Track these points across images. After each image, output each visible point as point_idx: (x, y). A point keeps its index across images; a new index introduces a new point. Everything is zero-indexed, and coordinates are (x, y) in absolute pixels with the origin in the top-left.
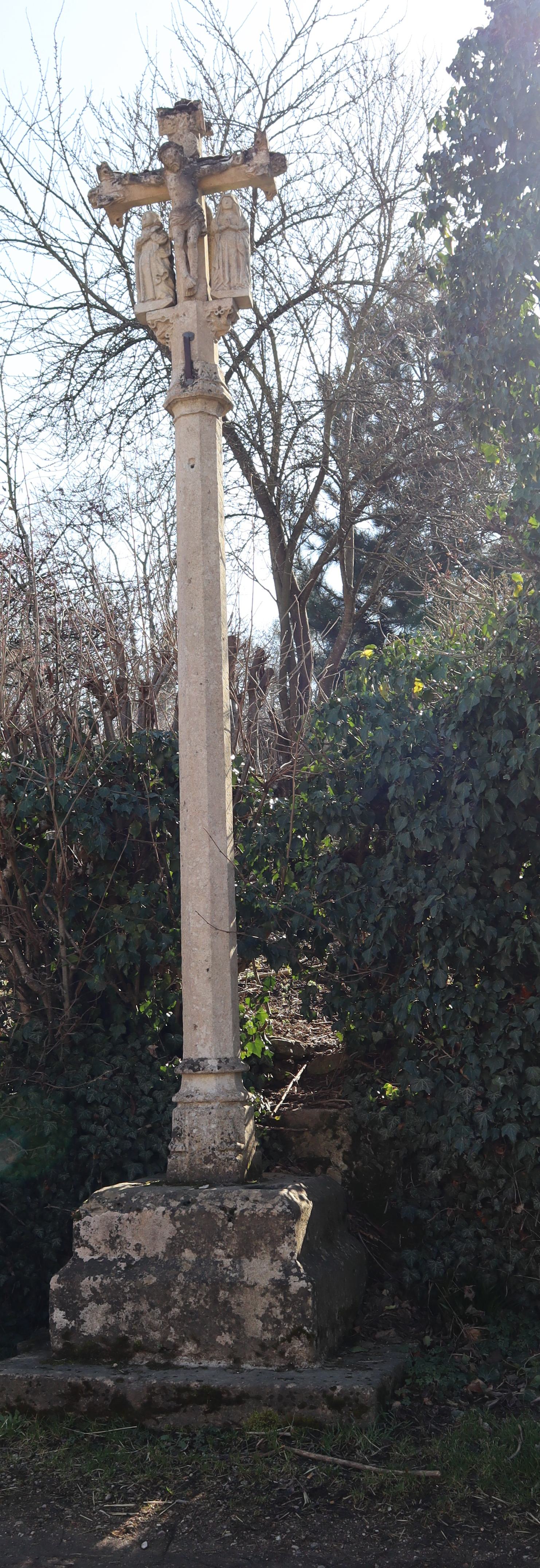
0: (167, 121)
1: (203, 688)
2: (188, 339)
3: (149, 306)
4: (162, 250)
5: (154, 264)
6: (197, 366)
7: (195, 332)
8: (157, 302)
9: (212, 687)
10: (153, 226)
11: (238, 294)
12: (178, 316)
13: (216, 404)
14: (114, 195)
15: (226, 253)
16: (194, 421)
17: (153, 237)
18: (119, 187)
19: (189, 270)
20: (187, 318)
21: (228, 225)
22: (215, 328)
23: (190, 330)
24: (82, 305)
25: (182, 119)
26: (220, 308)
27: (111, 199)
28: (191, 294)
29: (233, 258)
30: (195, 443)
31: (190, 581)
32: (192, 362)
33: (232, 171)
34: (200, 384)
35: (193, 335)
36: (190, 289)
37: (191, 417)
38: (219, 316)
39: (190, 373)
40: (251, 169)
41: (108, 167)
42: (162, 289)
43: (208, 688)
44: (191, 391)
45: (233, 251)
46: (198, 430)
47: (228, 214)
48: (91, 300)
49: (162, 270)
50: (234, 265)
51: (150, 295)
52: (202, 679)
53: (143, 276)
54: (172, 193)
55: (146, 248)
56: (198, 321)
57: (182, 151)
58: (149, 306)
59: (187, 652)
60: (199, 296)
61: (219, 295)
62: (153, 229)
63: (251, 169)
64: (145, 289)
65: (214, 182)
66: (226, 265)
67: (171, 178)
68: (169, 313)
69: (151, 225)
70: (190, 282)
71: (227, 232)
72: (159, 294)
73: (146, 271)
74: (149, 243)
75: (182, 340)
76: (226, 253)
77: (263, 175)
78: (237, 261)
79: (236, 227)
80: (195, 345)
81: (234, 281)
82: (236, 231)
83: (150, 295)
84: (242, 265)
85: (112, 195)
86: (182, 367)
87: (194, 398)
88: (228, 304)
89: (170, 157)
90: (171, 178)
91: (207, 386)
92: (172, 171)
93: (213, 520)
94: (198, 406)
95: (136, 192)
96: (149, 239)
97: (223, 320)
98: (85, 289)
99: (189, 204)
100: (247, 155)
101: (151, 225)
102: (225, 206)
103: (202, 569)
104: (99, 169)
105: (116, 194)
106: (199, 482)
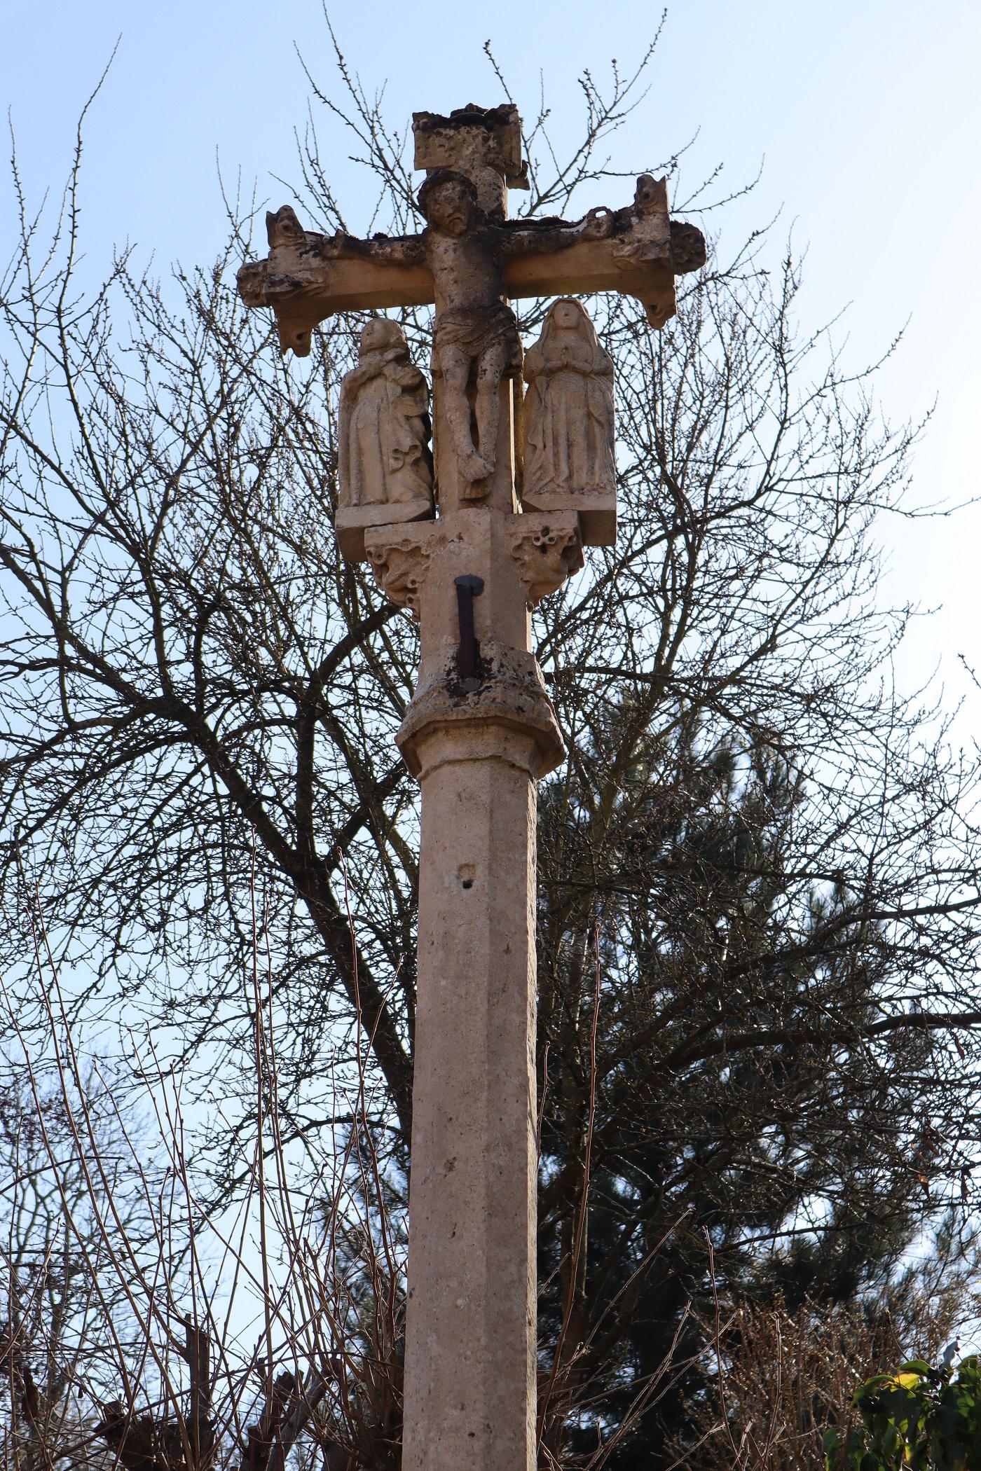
0: (437, 141)
1: (478, 1445)
2: (468, 590)
3: (372, 515)
4: (408, 399)
5: (387, 427)
6: (488, 651)
7: (486, 577)
8: (390, 507)
9: (500, 1445)
10: (386, 350)
11: (591, 503)
12: (443, 540)
13: (529, 743)
14: (300, 279)
15: (562, 415)
16: (477, 778)
17: (388, 371)
18: (315, 262)
19: (475, 441)
20: (468, 541)
21: (566, 359)
22: (530, 575)
23: (473, 570)
24: (50, 663)
25: (472, 143)
26: (546, 531)
27: (296, 284)
28: (479, 493)
29: (580, 427)
30: (477, 829)
31: (450, 1166)
32: (476, 644)
33: (582, 250)
34: (497, 692)
35: (481, 584)
36: (478, 483)
37: (469, 767)
38: (544, 549)
39: (470, 666)
40: (627, 250)
41: (293, 218)
42: (404, 482)
43: (489, 1447)
44: (472, 706)
45: (579, 414)
46: (485, 798)
47: (569, 338)
48: (74, 658)
49: (407, 442)
50: (580, 442)
51: (375, 493)
52: (475, 1421)
53: (360, 452)
54: (444, 278)
55: (372, 393)
56: (494, 555)
57: (474, 194)
58: (372, 515)
59: (435, 1349)
60: (494, 501)
61: (544, 501)
62: (390, 355)
63: (627, 250)
64: (361, 479)
65: (538, 269)
66: (562, 441)
67: (445, 250)
68: (420, 534)
69: (384, 347)
70: (478, 466)
71: (563, 376)
72: (396, 490)
73: (369, 441)
74: (378, 383)
75: (452, 592)
76: (562, 415)
77: (657, 261)
78: (589, 435)
79: (588, 368)
80: (484, 607)
81: (582, 478)
82: (585, 375)
83: (375, 493)
84: (599, 445)
85: (299, 276)
86: (451, 652)
87: (478, 724)
88: (566, 524)
89: (449, 200)
90: (445, 250)
91: (514, 698)
92: (448, 233)
93: (516, 1019)
94: (488, 743)
95: (356, 276)
96: (378, 374)
97: (553, 558)
98: (62, 630)
99: (486, 302)
100: (619, 222)
101: (384, 347)
102: (561, 320)
103: (485, 1137)
104: (271, 220)
105: (307, 275)
106: (483, 922)
